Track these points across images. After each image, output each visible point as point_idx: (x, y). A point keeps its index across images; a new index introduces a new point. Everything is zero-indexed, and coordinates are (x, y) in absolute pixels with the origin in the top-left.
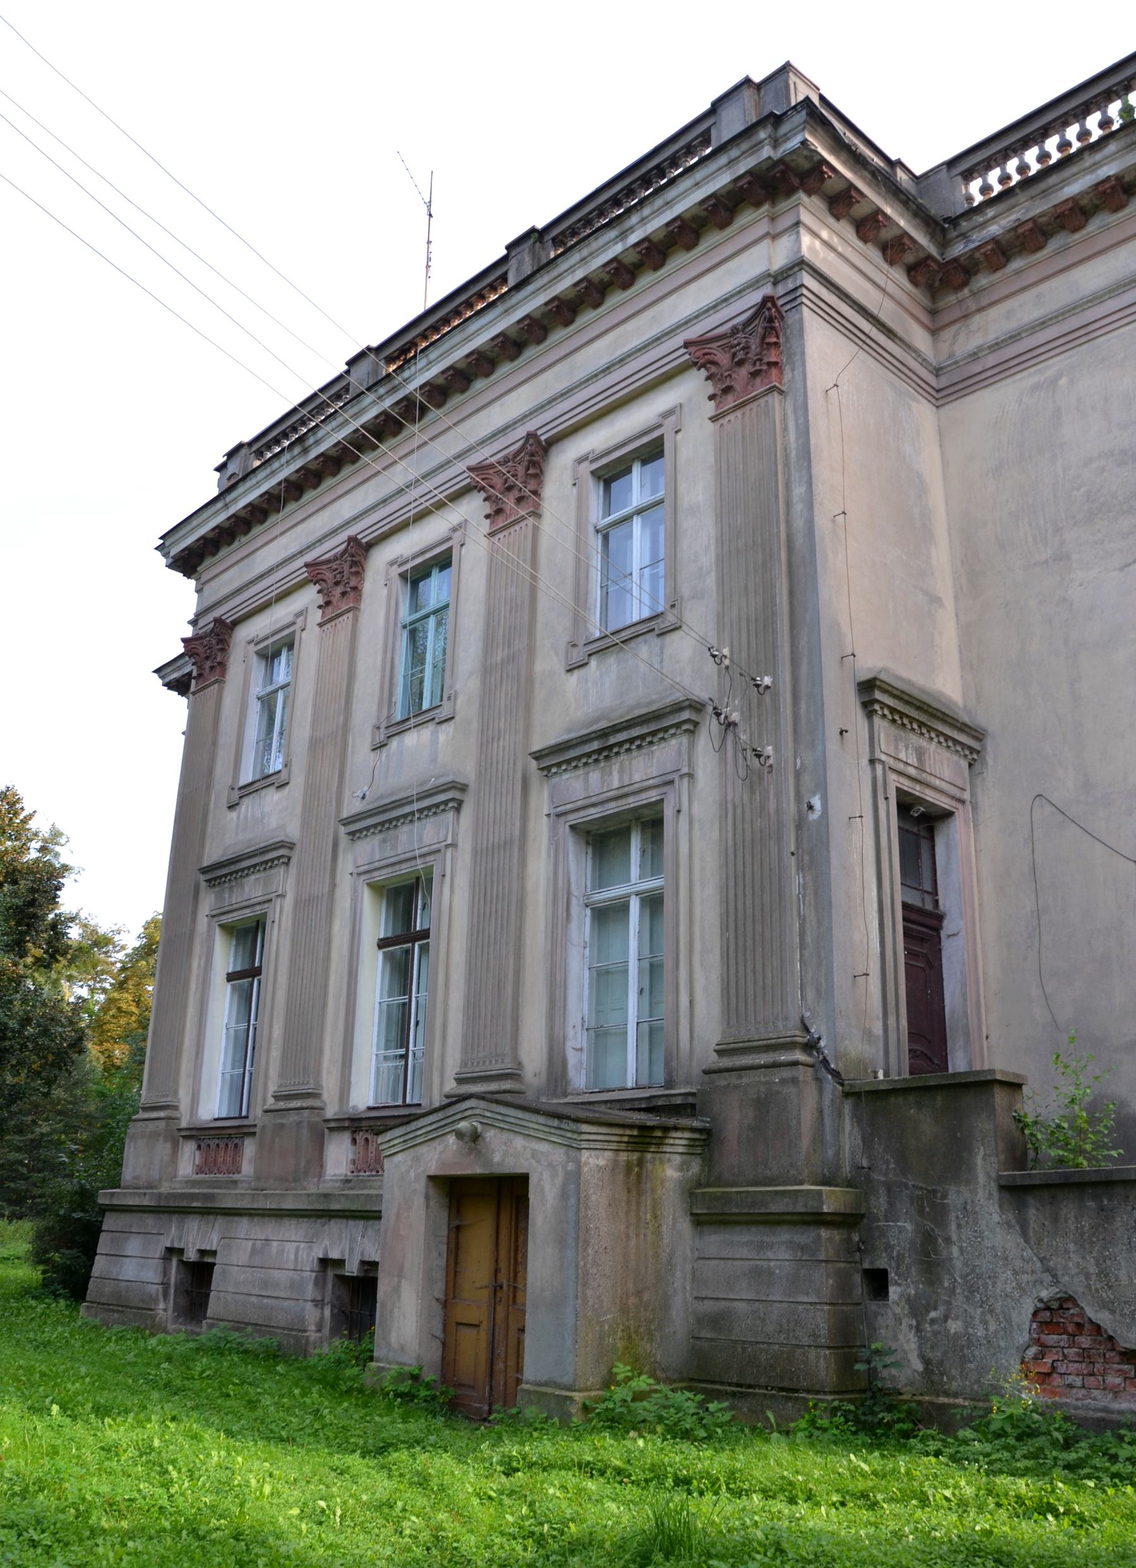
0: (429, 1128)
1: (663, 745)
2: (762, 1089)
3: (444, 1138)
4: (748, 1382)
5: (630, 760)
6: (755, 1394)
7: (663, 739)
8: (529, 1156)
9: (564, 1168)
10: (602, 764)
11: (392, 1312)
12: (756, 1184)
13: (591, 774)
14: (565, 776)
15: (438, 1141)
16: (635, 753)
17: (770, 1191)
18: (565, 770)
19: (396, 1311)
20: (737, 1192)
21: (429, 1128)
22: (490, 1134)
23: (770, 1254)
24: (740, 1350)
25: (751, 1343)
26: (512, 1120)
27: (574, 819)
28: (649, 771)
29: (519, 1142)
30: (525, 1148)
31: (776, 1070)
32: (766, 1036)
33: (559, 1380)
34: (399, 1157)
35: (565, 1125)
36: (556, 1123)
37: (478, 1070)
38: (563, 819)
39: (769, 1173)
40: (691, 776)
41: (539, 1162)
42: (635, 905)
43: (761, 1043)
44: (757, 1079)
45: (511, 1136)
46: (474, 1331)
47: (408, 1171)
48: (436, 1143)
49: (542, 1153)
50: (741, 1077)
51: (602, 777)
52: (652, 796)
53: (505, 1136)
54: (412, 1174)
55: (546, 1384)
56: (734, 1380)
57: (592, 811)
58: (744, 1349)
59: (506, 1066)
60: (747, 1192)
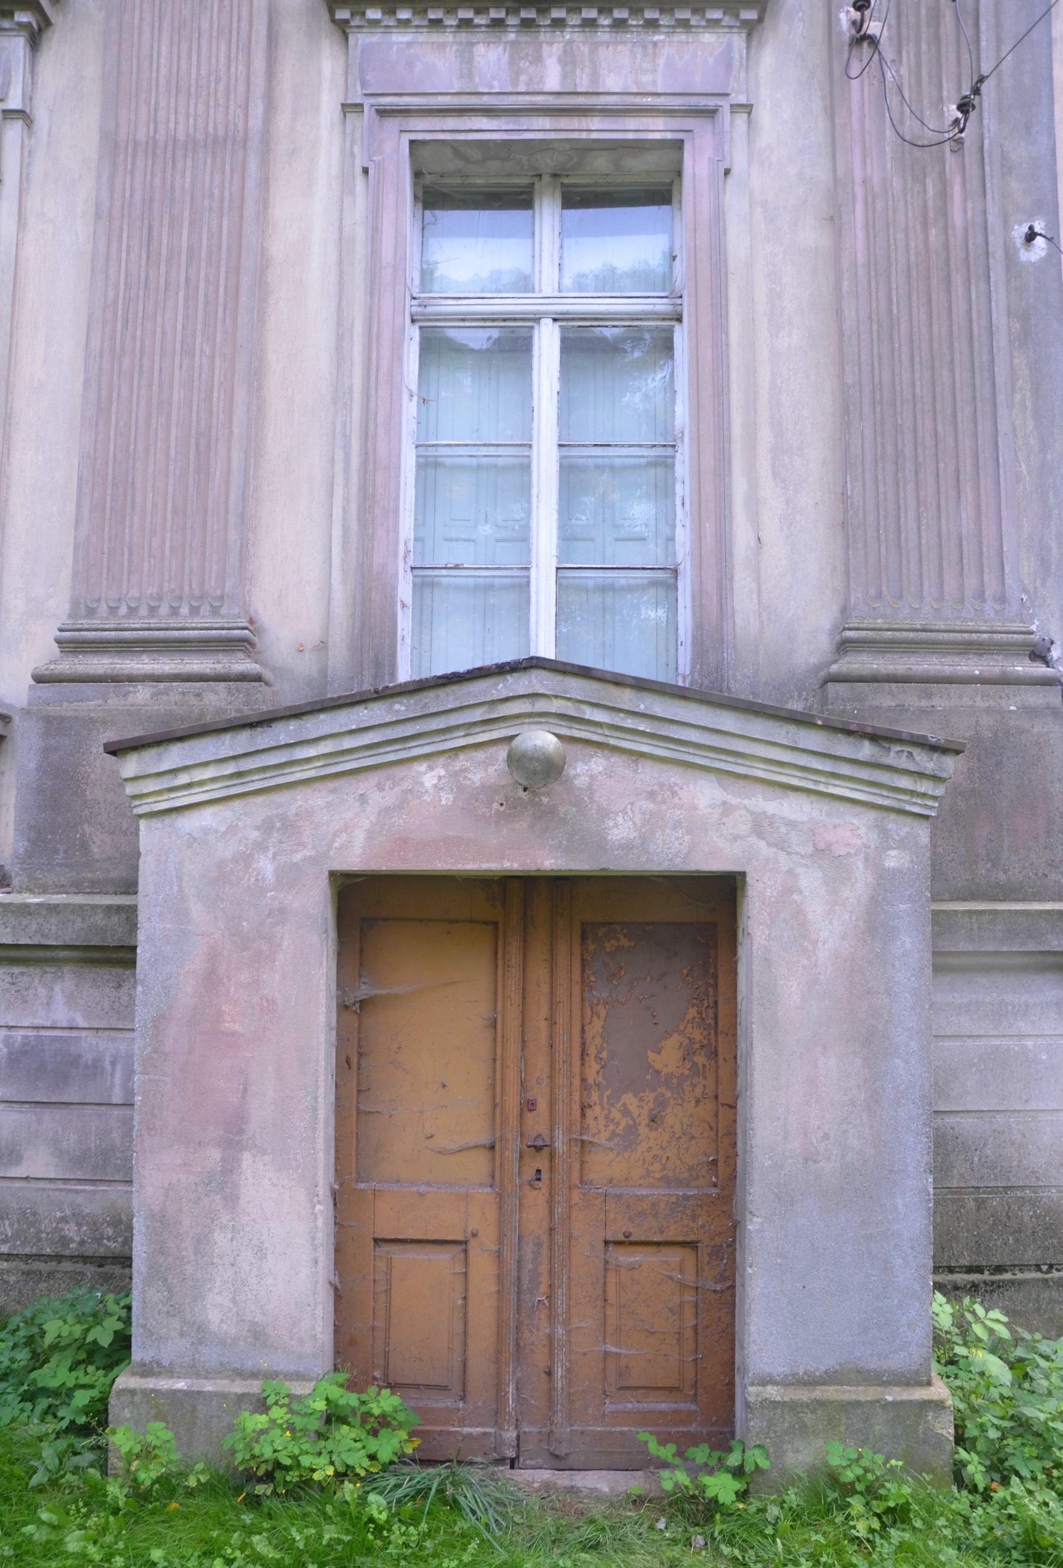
0: (348, 743)
1: (681, 36)
2: (986, 721)
3: (399, 772)
4: (996, 1261)
5: (595, 47)
6: (1021, 1283)
7: (685, 24)
8: (744, 828)
9: (873, 861)
10: (512, 36)
11: (202, 1241)
12: (972, 897)
13: (480, 49)
14: (400, 38)
15: (374, 778)
16: (603, 36)
17: (1048, 912)
18: (406, 23)
19: (221, 1238)
20: (970, 913)
21: (348, 743)
22: (587, 770)
23: (1023, 1026)
24: (971, 1204)
25: (993, 1190)
26: (693, 736)
27: (423, 128)
28: (646, 79)
29: (704, 794)
30: (727, 809)
31: (1009, 689)
32: (958, 625)
33: (874, 1364)
34: (206, 818)
35: (894, 756)
36: (866, 750)
37: (102, 624)
38: (393, 124)
39: (1002, 876)
40: (747, 108)
41: (781, 845)
42: (547, 342)
43: (958, 636)
44: (966, 701)
45: (674, 776)
46: (443, 1257)
47: (246, 859)
48: (366, 784)
49: (791, 824)
50: (929, 696)
51: (512, 62)
52: (657, 129)
53: (648, 774)
54: (266, 865)
55: (830, 1378)
56: (965, 1262)
57: (483, 122)
58: (981, 1204)
59: (226, 621)
60: (995, 913)
